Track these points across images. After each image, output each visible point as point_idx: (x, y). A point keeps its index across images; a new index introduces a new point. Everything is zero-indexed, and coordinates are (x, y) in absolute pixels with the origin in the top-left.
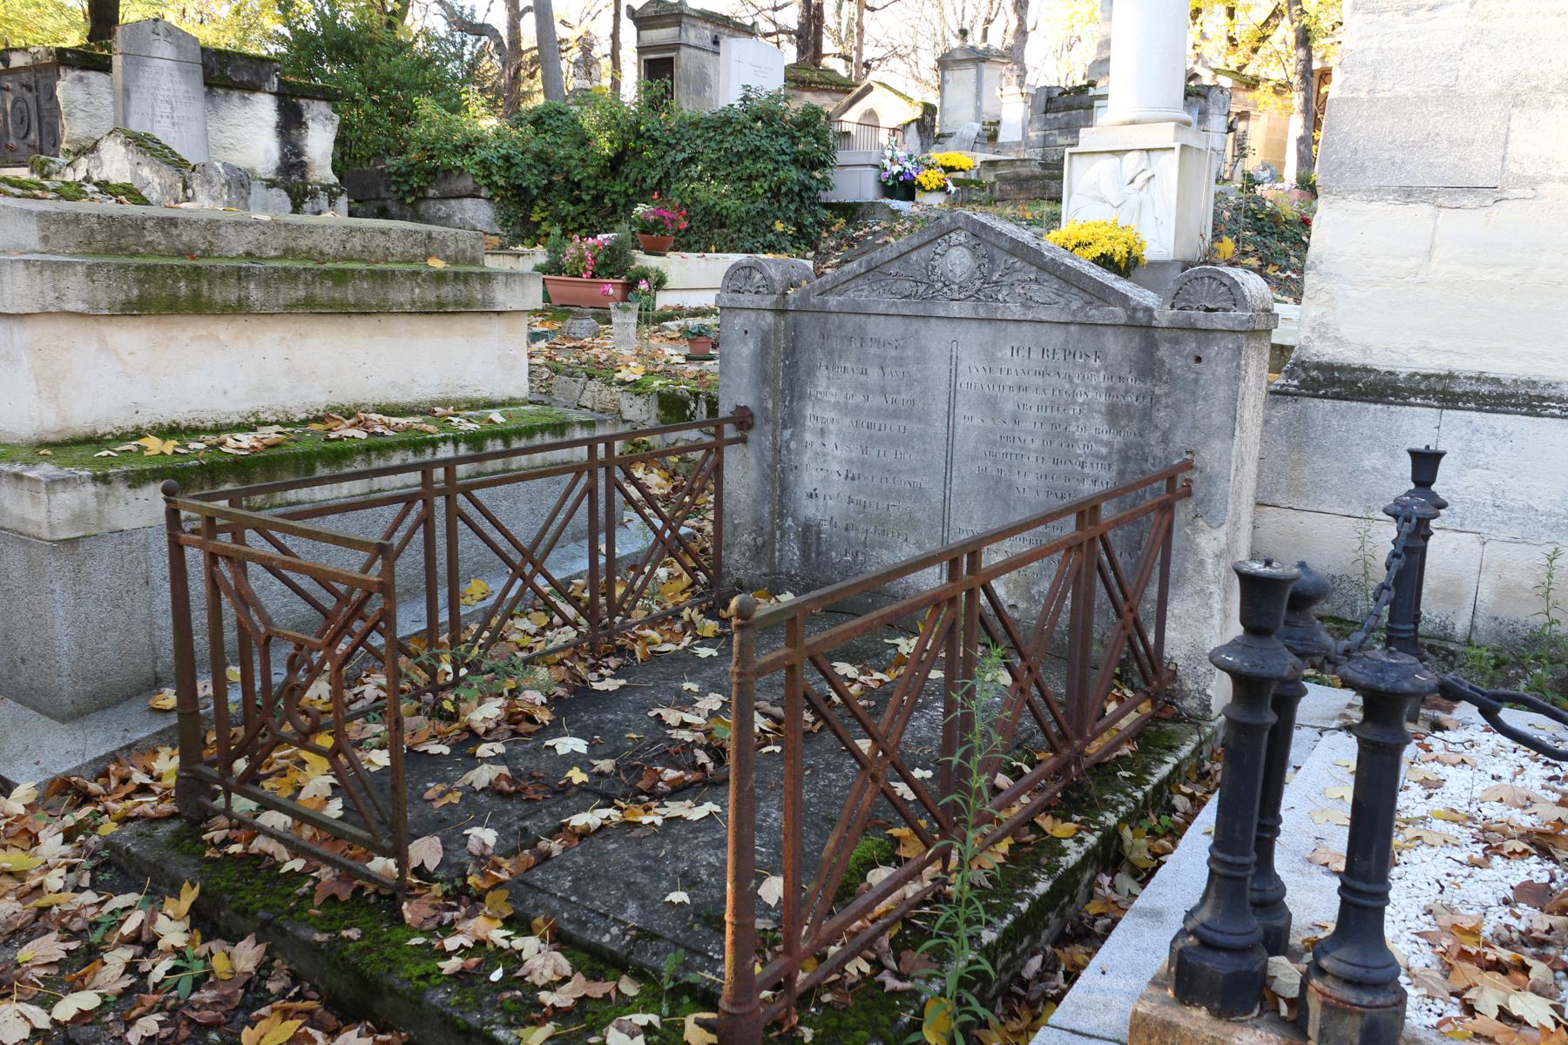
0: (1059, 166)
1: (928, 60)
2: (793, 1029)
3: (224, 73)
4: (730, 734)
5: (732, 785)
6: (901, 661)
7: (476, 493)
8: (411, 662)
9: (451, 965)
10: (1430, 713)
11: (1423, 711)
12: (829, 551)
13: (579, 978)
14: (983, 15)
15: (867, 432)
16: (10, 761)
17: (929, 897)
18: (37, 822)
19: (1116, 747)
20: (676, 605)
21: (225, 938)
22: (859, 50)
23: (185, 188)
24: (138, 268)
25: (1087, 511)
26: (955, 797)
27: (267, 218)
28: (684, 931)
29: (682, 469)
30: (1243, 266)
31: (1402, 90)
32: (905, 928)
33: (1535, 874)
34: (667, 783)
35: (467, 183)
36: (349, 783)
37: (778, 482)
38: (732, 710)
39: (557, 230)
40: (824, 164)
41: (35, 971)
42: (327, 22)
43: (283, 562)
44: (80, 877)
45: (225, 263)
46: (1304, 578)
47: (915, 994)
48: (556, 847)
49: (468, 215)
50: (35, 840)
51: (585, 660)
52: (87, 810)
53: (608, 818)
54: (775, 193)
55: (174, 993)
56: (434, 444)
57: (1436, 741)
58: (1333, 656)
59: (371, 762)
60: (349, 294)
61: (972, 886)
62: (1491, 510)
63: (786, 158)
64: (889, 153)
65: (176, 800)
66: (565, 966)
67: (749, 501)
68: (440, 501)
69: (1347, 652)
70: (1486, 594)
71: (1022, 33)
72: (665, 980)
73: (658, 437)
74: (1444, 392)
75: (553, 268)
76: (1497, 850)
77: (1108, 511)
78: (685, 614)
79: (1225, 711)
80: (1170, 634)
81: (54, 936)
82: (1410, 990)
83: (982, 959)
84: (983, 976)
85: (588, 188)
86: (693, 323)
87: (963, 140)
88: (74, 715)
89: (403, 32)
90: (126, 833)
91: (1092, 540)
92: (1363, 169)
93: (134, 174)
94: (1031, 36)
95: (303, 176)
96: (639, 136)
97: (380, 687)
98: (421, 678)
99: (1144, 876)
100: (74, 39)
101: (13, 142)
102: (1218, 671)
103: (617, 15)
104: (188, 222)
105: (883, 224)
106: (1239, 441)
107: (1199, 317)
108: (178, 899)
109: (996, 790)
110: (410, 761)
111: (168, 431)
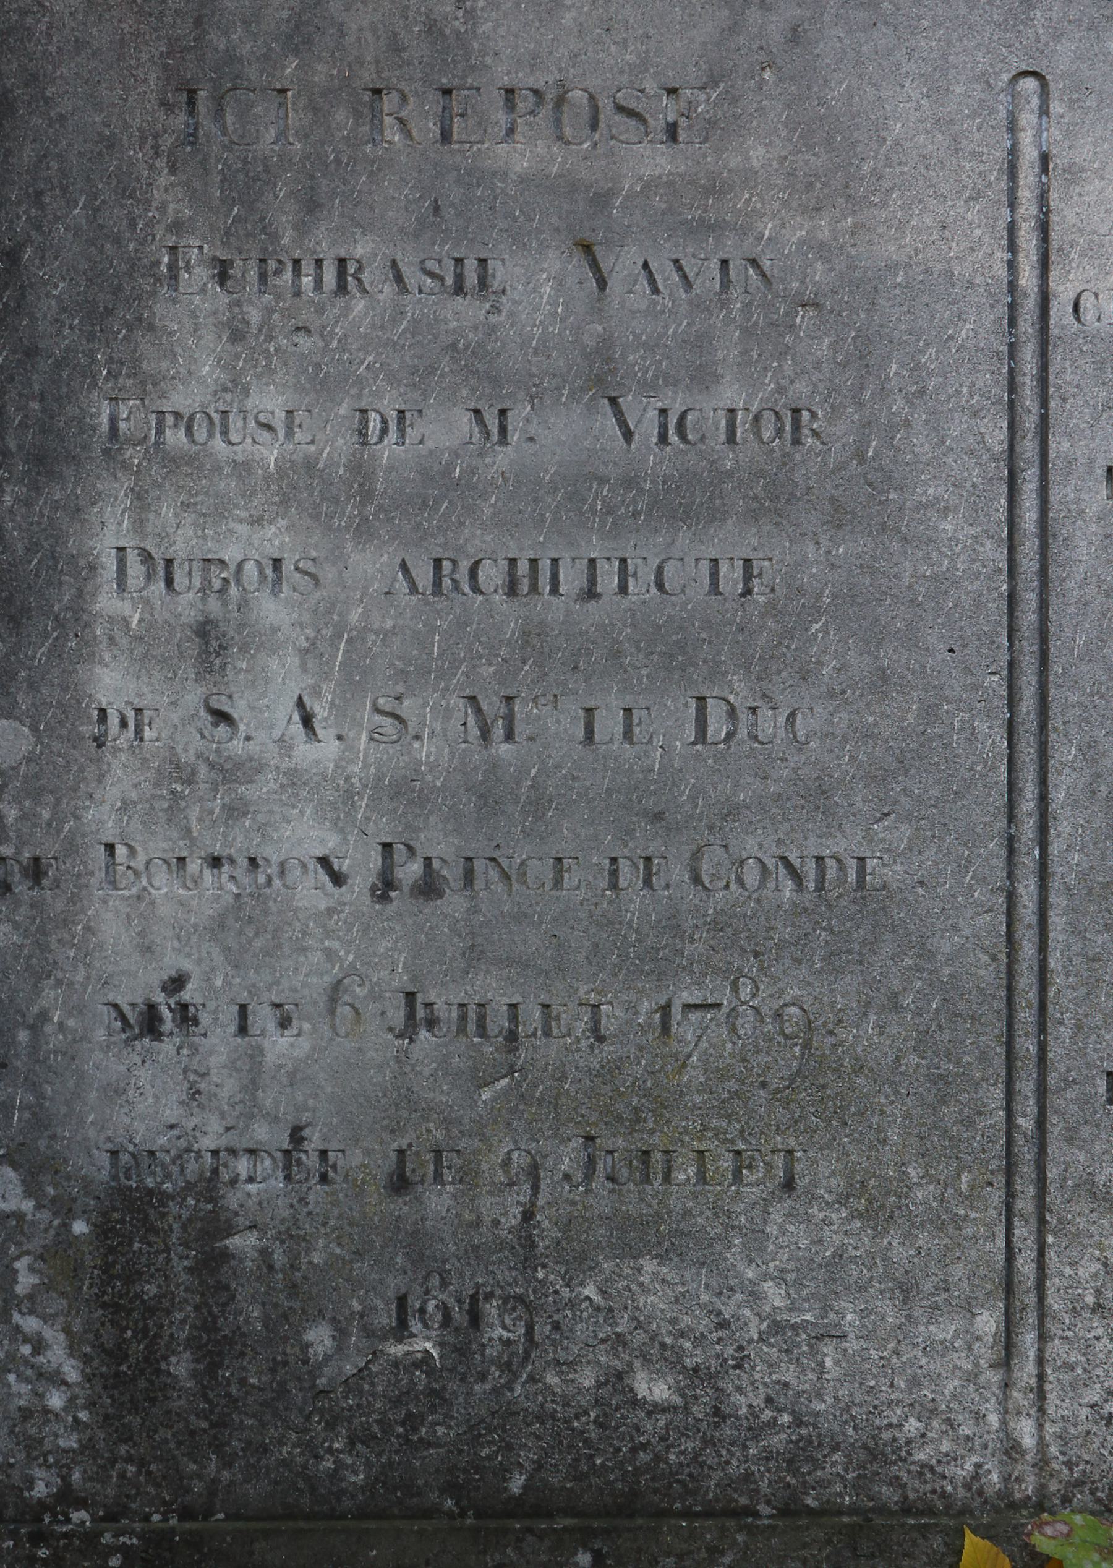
15: (510, 616)
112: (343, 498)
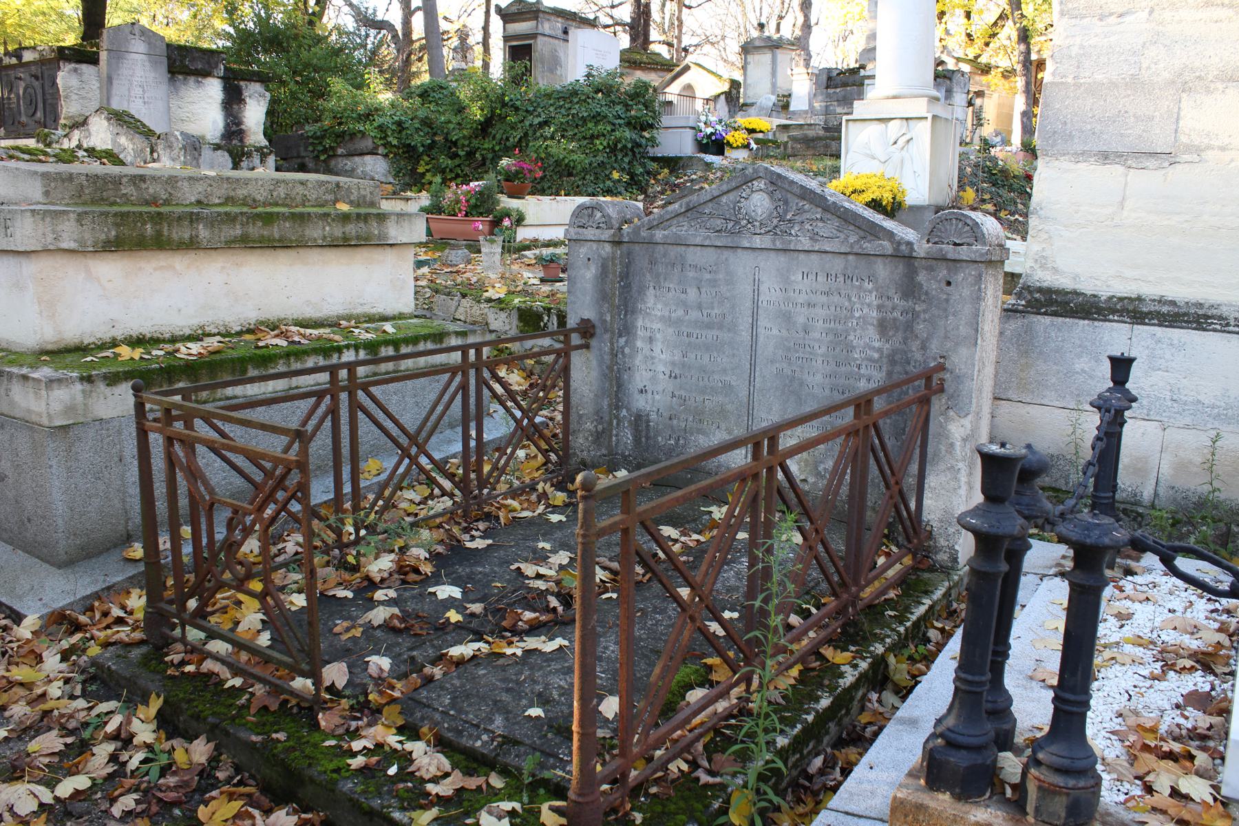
0: (838, 129)
1: (734, 47)
2: (627, 814)
3: (183, 63)
4: (576, 583)
5: (577, 624)
6: (714, 525)
7: (373, 389)
8: (322, 524)
9: (359, 761)
10: (1124, 561)
11: (1118, 560)
12: (656, 436)
13: (457, 774)
14: (777, 12)
16: (20, 598)
17: (735, 712)
18: (41, 645)
19: (884, 592)
20: (532, 479)
21: (183, 737)
22: (679, 38)
23: (152, 152)
24: (115, 215)
25: (862, 404)
26: (757, 633)
27: (213, 174)
28: (540, 738)
29: (537, 369)
30: (982, 211)
31: (1099, 77)
32: (716, 736)
33: (1200, 685)
34: (526, 622)
35: (368, 144)
36: (275, 619)
37: (615, 380)
38: (578, 564)
39: (438, 179)
40: (651, 126)
41: (41, 759)
42: (262, 22)
43: (223, 444)
44: (74, 688)
45: (180, 210)
46: (1030, 456)
47: (723, 787)
48: (437, 672)
49: (368, 168)
50: (39, 659)
51: (459, 524)
52: (78, 636)
53: (479, 650)
54: (613, 149)
55: (146, 778)
56: (339, 350)
57: (1127, 583)
58: (1051, 518)
59: (291, 603)
60: (275, 231)
61: (770, 703)
62: (1170, 403)
63: (622, 122)
64: (703, 118)
65: (144, 630)
66: (446, 764)
67: (591, 395)
68: (344, 396)
69: (1062, 515)
70: (1166, 469)
71: (807, 27)
72: (525, 776)
73: (518, 344)
74: (1134, 311)
75: (435, 209)
76: (1172, 667)
77: (879, 404)
78: (540, 487)
79: (969, 562)
80: (927, 502)
81: (55, 732)
82: (1104, 775)
83: (776, 759)
84: (777, 772)
85: (463, 146)
86: (546, 252)
87: (761, 109)
88: (67, 563)
89: (321, 28)
90: (107, 655)
91: (867, 427)
92: (1071, 136)
93: (114, 142)
94: (814, 29)
95: (241, 140)
96: (504, 105)
97: (298, 544)
98: (330, 537)
99: (904, 693)
100: (71, 40)
101: (24, 119)
102: (964, 531)
103: (487, 13)
104: (153, 178)
105: (699, 173)
106: (980, 349)
107: (949, 250)
108: (148, 706)
109: (789, 627)
110: (322, 602)
111: (137, 341)
112: (667, 321)
